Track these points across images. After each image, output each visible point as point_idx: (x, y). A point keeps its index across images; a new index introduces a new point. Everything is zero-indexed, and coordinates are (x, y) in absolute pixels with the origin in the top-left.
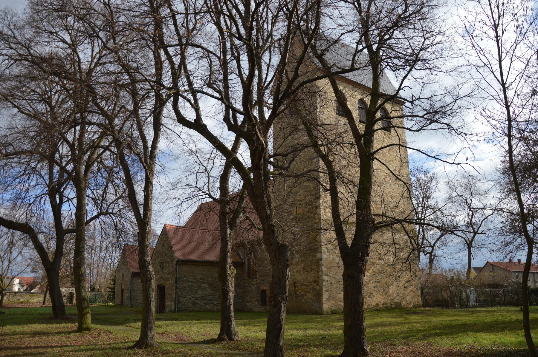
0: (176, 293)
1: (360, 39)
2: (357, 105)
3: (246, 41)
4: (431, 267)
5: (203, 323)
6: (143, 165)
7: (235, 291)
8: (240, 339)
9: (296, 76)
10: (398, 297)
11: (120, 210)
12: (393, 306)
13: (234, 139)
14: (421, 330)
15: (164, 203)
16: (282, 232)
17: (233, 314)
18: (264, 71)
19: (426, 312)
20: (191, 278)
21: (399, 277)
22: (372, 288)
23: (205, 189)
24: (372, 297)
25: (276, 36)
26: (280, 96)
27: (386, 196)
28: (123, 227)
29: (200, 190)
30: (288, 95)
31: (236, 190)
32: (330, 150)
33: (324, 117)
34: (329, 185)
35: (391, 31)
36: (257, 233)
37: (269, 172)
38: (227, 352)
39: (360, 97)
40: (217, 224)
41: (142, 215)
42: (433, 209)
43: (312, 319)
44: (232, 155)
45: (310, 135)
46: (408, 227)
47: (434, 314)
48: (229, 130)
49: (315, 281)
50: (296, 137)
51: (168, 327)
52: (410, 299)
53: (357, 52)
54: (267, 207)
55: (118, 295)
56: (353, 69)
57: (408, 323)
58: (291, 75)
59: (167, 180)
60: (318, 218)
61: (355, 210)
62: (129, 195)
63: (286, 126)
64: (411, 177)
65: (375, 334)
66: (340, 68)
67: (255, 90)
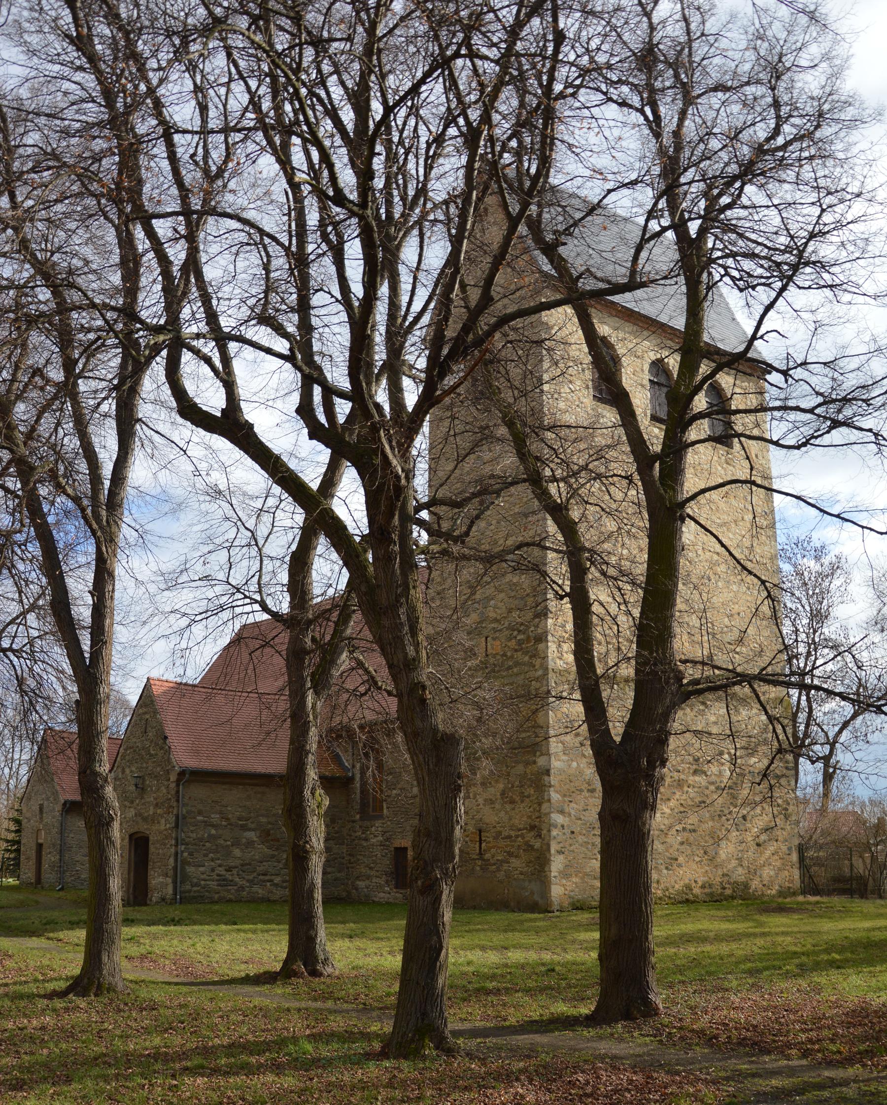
0: (176, 854)
1: (656, 204)
2: (646, 377)
3: (355, 209)
4: (826, 794)
5: (245, 931)
6: (90, 527)
7: (328, 849)
8: (337, 973)
9: (486, 300)
10: (740, 869)
11: (31, 643)
12: (728, 892)
13: (327, 461)
14: (795, 953)
15: (145, 623)
16: (448, 700)
17: (320, 910)
18: (405, 286)
19: (810, 907)
20: (215, 818)
21: (744, 818)
22: (676, 846)
23: (252, 589)
24: (674, 866)
25: (439, 190)
26: (445, 351)
27: (714, 614)
28: (40, 684)
29: (238, 590)
30: (466, 349)
31: (331, 592)
32: (574, 493)
33: (562, 405)
34: (568, 583)
35: (737, 185)
36: (384, 704)
37: (416, 543)
38: (303, 1005)
39: (653, 356)
40: (283, 680)
41: (87, 655)
42: (835, 647)
43: (521, 922)
44: (319, 504)
45: (522, 454)
46: (772, 692)
47: (829, 913)
48: (311, 438)
49: (533, 828)
50: (487, 456)
51: (156, 943)
52: (772, 873)
53: (646, 239)
54: (408, 638)
55: (28, 859)
56: (632, 285)
57: (764, 934)
58: (474, 295)
59: (153, 566)
60: (541, 665)
61: (634, 646)
62: (53, 604)
63: (460, 428)
64: (782, 565)
65: (678, 962)
66: (601, 280)
67: (379, 338)
